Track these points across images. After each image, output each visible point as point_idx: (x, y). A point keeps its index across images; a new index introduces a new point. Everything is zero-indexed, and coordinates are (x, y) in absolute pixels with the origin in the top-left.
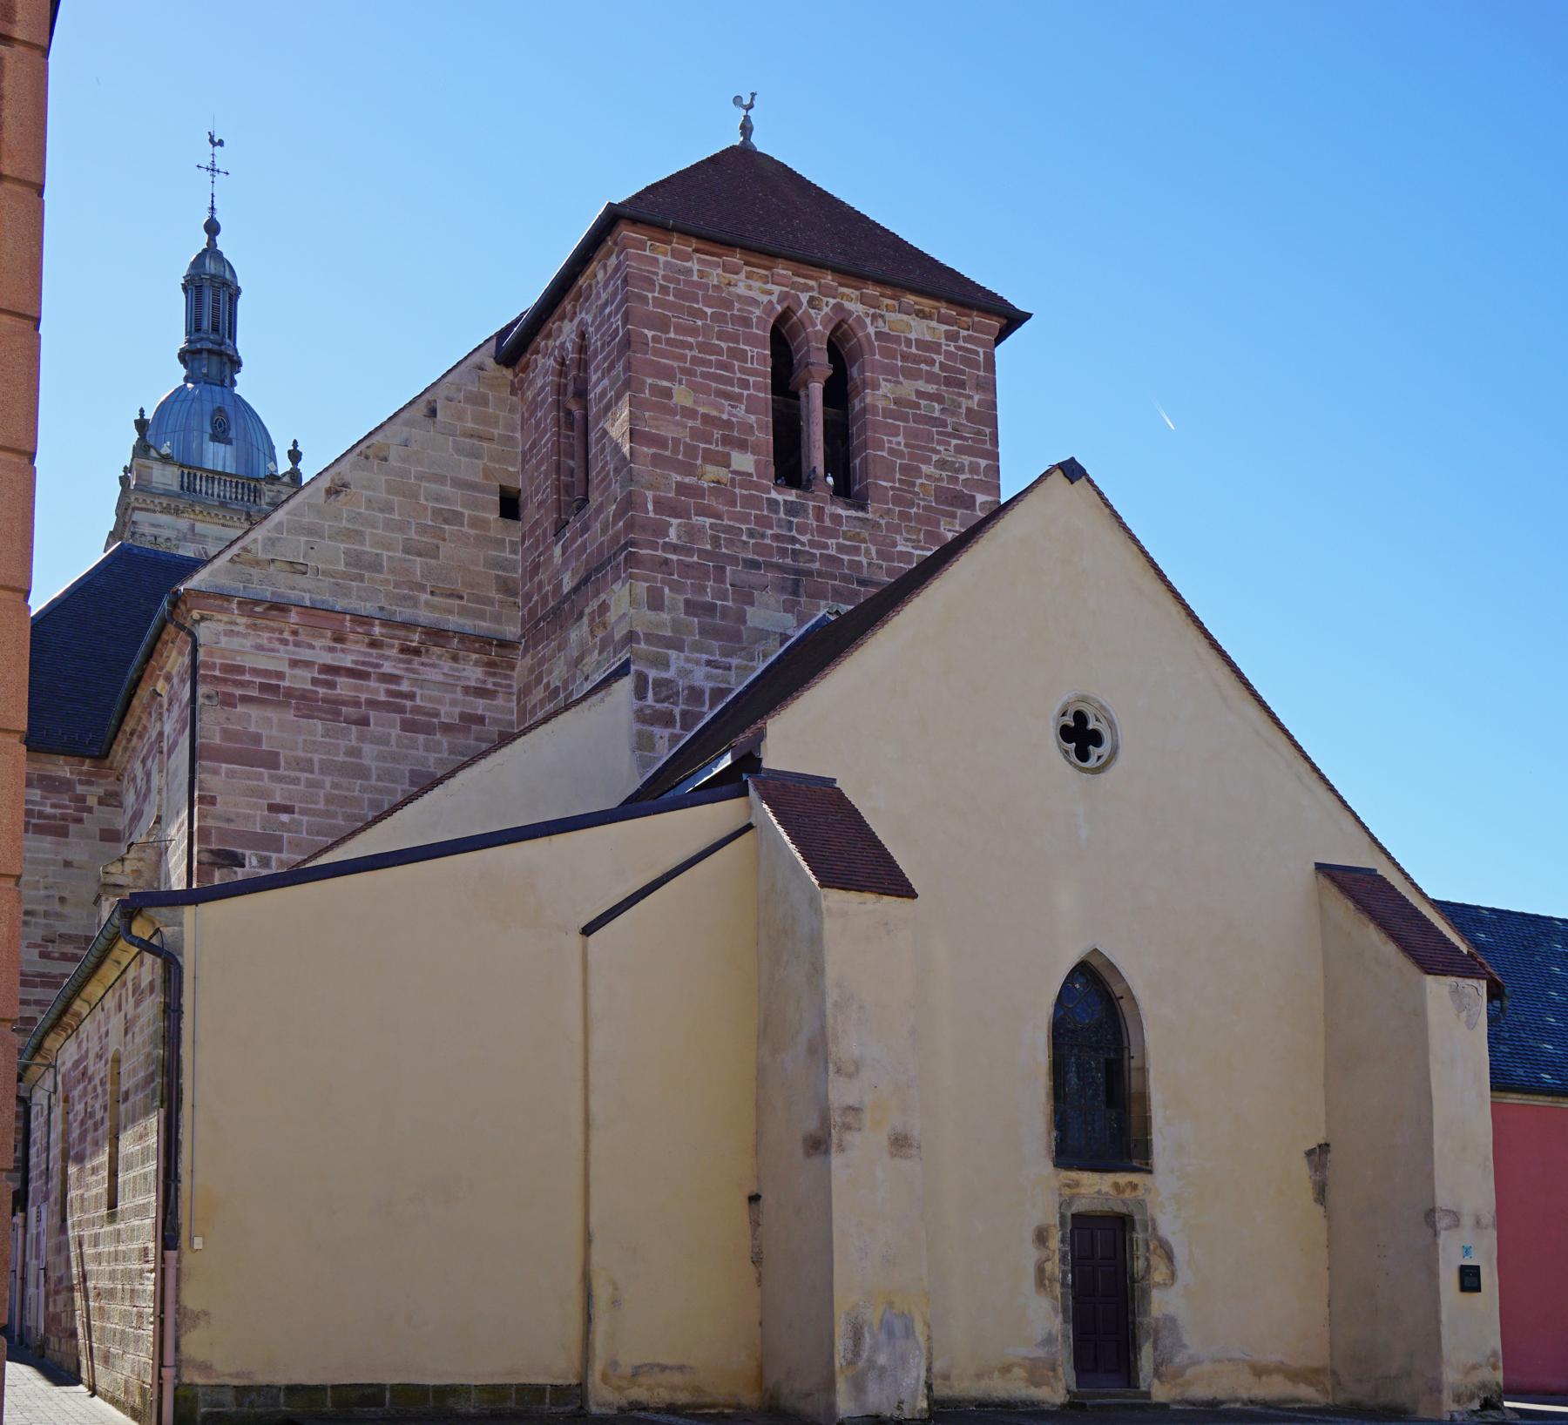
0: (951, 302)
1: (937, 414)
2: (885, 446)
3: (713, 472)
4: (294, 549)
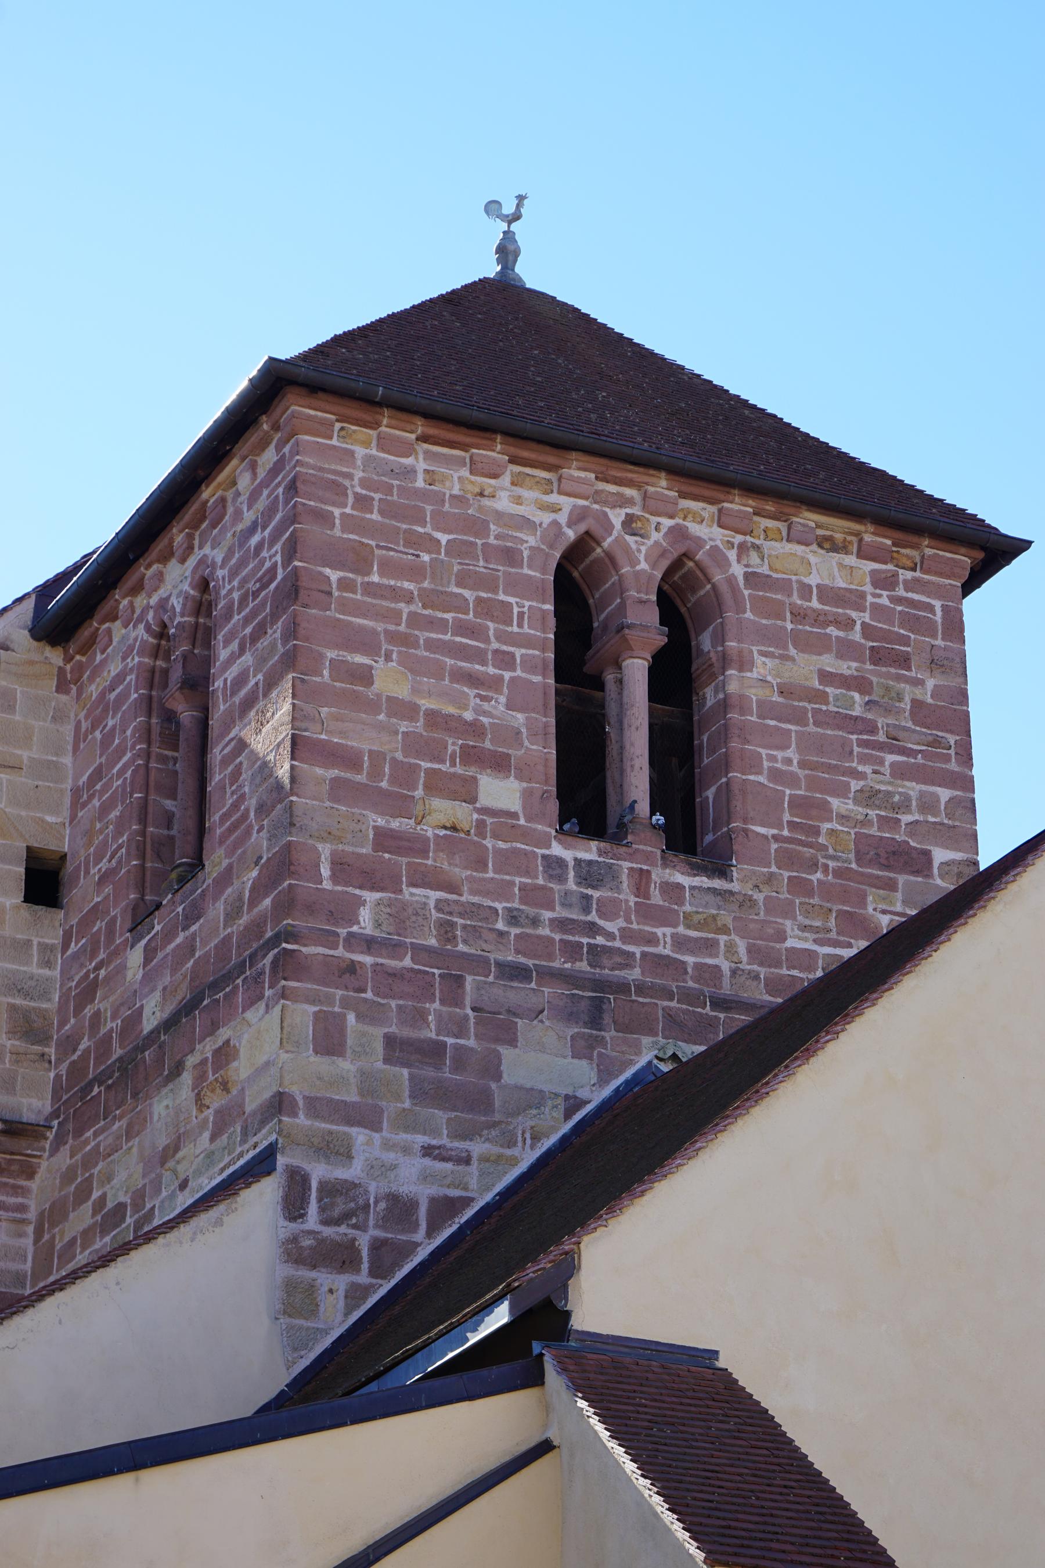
0: (883, 522)
3: (444, 810)
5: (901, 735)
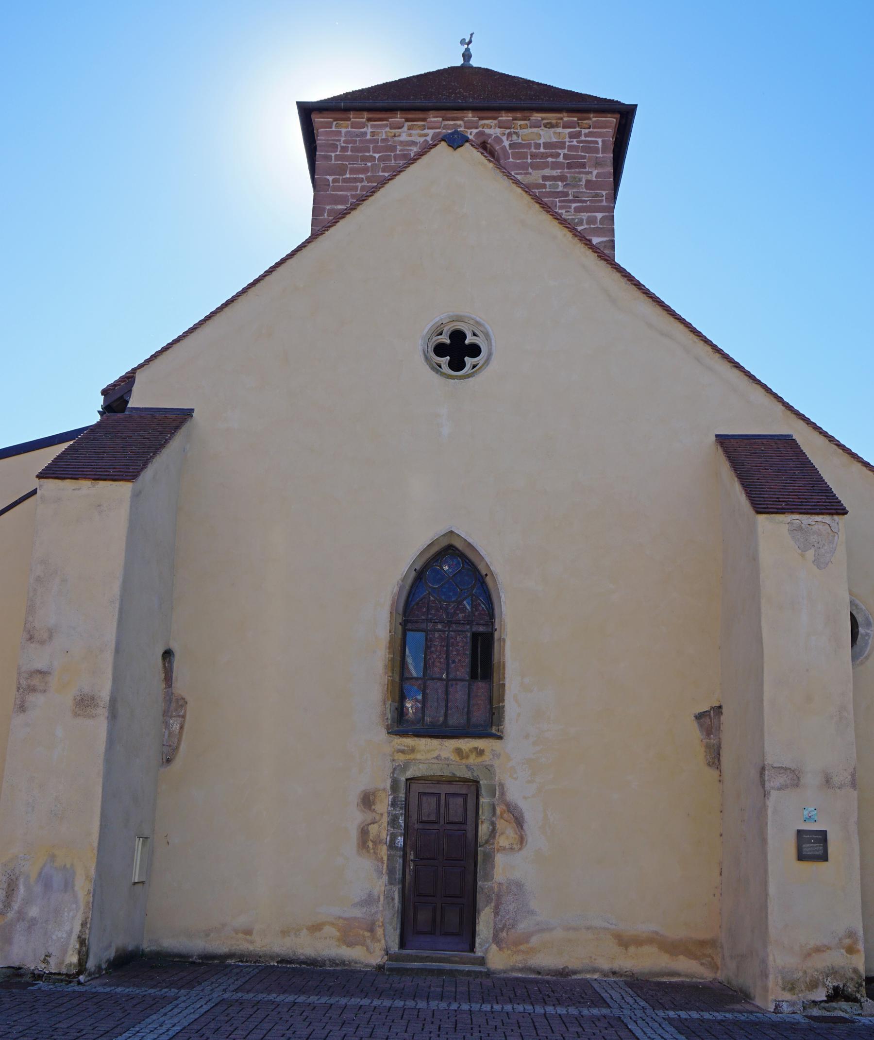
0: (571, 111)
1: (560, 189)
5: (580, 195)
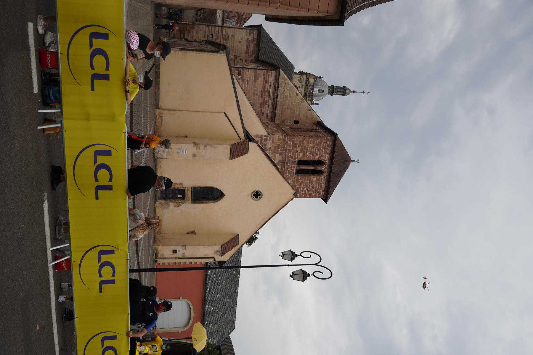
2: (305, 179)
3: (299, 150)
4: (288, 87)
